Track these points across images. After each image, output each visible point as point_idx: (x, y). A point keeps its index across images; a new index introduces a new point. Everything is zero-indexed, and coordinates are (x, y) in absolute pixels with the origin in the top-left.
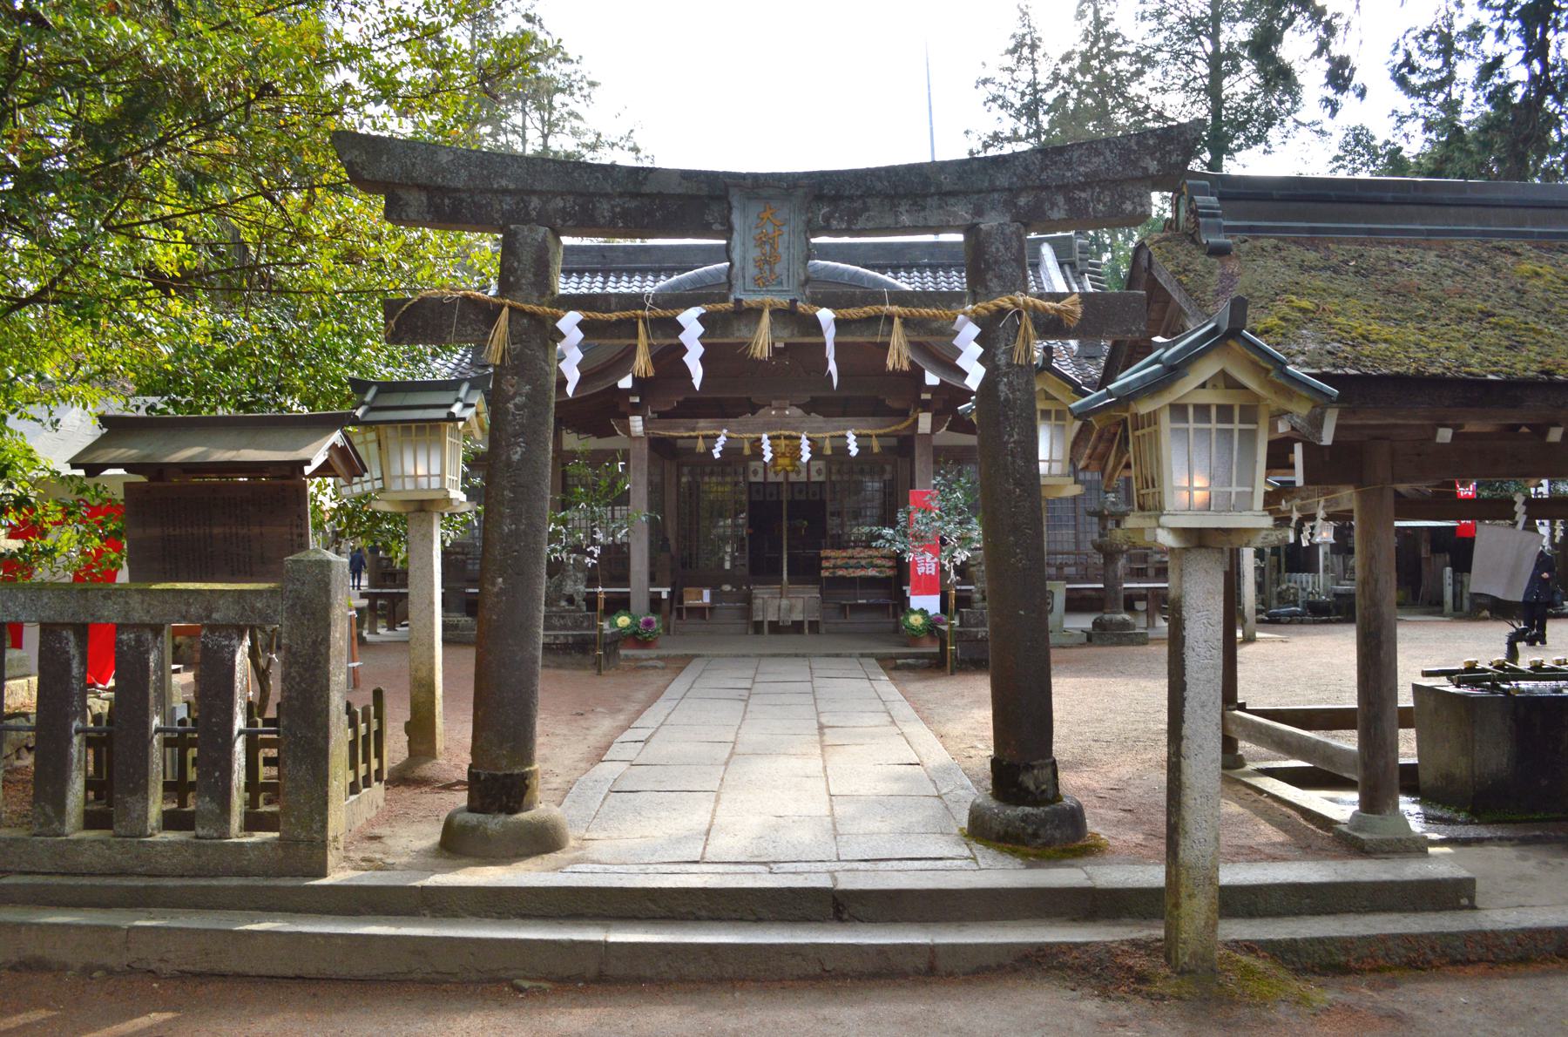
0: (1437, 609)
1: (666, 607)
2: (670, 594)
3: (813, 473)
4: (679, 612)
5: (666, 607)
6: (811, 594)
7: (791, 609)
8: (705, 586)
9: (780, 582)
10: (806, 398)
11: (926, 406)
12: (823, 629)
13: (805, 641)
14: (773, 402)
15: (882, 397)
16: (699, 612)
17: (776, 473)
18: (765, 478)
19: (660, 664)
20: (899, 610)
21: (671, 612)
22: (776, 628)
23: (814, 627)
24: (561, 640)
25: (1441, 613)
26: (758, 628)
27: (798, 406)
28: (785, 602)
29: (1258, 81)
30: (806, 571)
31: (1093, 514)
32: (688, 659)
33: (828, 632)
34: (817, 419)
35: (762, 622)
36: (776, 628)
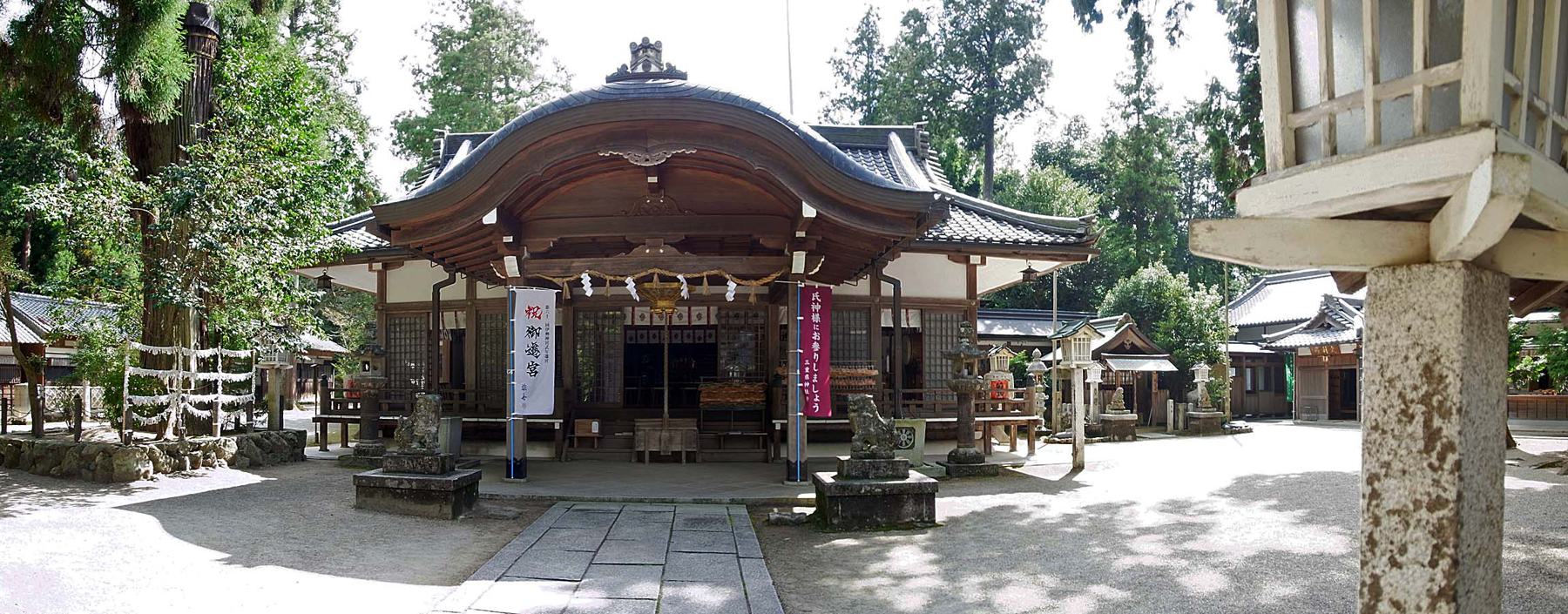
0: (1163, 428)
1: (559, 436)
2: (564, 426)
3: (694, 318)
4: (571, 440)
5: (559, 436)
6: (689, 426)
7: (671, 440)
8: (594, 418)
9: (660, 415)
10: (682, 236)
11: (799, 245)
12: (699, 458)
13: (683, 469)
14: (1236, 330)
15: (756, 236)
16: (587, 441)
17: (661, 318)
18: (633, 322)
19: (513, 510)
20: (769, 440)
21: (564, 440)
22: (656, 458)
23: (691, 458)
24: (406, 486)
25: (1165, 431)
26: (640, 457)
27: (671, 245)
28: (665, 434)
29: (1029, 99)
30: (685, 404)
31: (949, 356)
32: (546, 504)
33: (704, 461)
34: (690, 258)
35: (644, 452)
36: (656, 458)
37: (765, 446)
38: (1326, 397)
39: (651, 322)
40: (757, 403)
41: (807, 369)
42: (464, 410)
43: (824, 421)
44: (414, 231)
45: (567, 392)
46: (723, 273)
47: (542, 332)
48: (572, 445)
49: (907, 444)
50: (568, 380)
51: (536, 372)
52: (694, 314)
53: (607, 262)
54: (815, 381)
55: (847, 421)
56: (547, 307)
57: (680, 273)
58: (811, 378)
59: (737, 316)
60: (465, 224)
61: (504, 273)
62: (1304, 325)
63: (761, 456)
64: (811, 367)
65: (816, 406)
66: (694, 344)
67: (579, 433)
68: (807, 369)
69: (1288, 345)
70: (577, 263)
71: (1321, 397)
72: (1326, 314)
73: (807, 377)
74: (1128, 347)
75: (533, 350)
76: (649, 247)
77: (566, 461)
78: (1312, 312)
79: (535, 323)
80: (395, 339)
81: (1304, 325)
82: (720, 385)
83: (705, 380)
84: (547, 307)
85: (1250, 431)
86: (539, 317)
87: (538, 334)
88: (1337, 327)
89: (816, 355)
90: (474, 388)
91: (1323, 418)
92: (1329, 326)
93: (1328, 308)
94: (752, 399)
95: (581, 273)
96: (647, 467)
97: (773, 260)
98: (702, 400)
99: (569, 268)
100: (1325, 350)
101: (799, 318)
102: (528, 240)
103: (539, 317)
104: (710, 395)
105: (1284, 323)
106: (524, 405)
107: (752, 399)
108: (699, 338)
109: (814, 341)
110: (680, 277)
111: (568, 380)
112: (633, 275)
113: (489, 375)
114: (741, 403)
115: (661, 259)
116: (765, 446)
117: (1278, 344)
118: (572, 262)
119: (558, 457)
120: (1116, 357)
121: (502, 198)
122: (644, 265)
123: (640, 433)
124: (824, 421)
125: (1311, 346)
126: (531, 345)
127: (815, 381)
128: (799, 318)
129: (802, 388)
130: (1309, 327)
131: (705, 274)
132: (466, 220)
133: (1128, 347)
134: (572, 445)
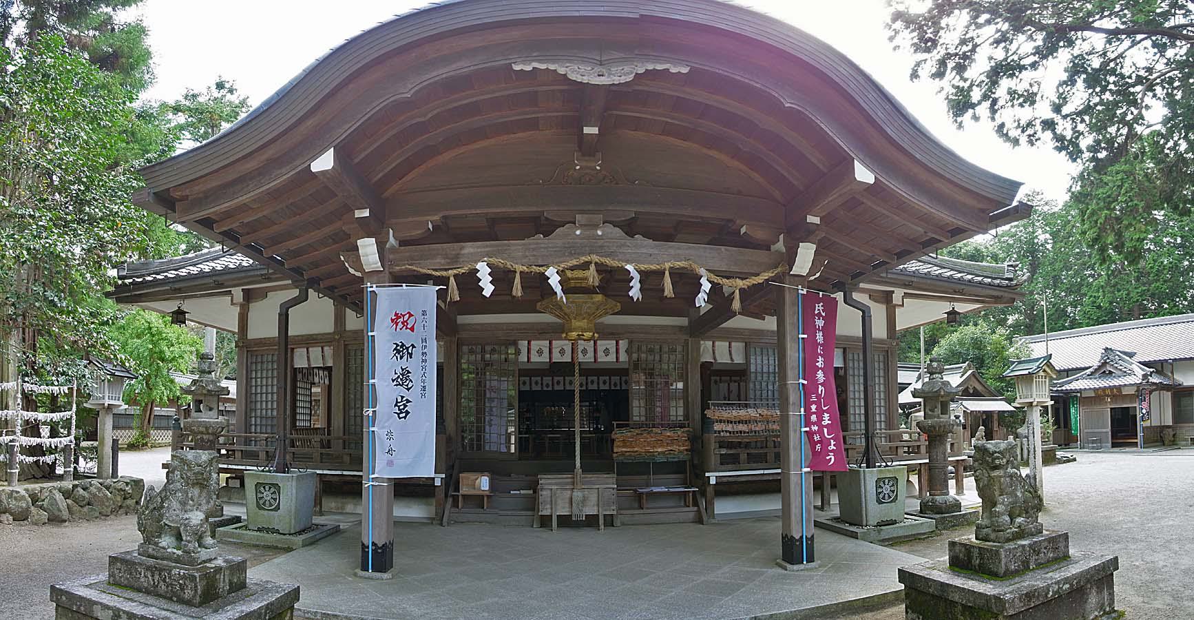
2: (446, 482)
3: (600, 353)
4: (455, 499)
6: (606, 484)
7: (584, 500)
12: (617, 522)
13: (601, 536)
16: (478, 501)
20: (698, 496)
23: (610, 521)
26: (545, 522)
33: (623, 524)
37: (696, 504)
38: (1109, 429)
39: (550, 358)
40: (680, 452)
41: (814, 407)
42: (325, 460)
43: (766, 472)
44: (206, 197)
45: (449, 440)
46: (695, 266)
47: (417, 353)
48: (455, 504)
49: (890, 497)
50: (451, 425)
51: (407, 413)
52: (600, 349)
53: (517, 246)
54: (826, 422)
55: (779, 471)
56: (424, 313)
57: (628, 262)
58: (820, 419)
59: (651, 351)
60: (283, 176)
61: (359, 267)
62: (1088, 371)
63: (691, 515)
64: (818, 403)
65: (832, 457)
66: (542, 391)
67: (464, 490)
68: (814, 407)
69: (1073, 388)
70: (469, 248)
71: (1104, 430)
72: (1108, 363)
73: (814, 418)
74: (971, 391)
75: (403, 378)
76: (581, 226)
77: (449, 524)
78: (1095, 363)
79: (407, 338)
80: (256, 386)
81: (1088, 371)
82: (637, 431)
83: (619, 426)
84: (424, 313)
85: (1075, 460)
86: (412, 329)
87: (411, 355)
88: (1119, 373)
89: (820, 388)
90: (341, 434)
91: (1106, 447)
92: (1111, 373)
93: (1108, 358)
94: (675, 447)
95: (476, 262)
96: (557, 535)
97: (760, 256)
98: (615, 450)
99: (457, 256)
100: (1108, 392)
101: (801, 336)
102: (394, 221)
103: (412, 329)
104: (626, 444)
105: (1073, 370)
106: (390, 463)
107: (675, 447)
108: (547, 386)
109: (818, 369)
110: (629, 267)
111: (451, 425)
112: (558, 264)
113: (264, 411)
114: (663, 453)
115: (600, 243)
116: (696, 504)
117: (1067, 387)
118: (462, 248)
119: (438, 519)
120: (970, 400)
121: (344, 131)
122: (573, 251)
123: (544, 493)
124: (766, 472)
125: (1095, 390)
126: (399, 371)
127: (826, 422)
128: (801, 336)
129: (810, 434)
130: (1092, 373)
131: (667, 265)
132: (284, 170)
133: (971, 391)
134: (455, 504)
